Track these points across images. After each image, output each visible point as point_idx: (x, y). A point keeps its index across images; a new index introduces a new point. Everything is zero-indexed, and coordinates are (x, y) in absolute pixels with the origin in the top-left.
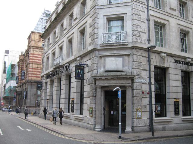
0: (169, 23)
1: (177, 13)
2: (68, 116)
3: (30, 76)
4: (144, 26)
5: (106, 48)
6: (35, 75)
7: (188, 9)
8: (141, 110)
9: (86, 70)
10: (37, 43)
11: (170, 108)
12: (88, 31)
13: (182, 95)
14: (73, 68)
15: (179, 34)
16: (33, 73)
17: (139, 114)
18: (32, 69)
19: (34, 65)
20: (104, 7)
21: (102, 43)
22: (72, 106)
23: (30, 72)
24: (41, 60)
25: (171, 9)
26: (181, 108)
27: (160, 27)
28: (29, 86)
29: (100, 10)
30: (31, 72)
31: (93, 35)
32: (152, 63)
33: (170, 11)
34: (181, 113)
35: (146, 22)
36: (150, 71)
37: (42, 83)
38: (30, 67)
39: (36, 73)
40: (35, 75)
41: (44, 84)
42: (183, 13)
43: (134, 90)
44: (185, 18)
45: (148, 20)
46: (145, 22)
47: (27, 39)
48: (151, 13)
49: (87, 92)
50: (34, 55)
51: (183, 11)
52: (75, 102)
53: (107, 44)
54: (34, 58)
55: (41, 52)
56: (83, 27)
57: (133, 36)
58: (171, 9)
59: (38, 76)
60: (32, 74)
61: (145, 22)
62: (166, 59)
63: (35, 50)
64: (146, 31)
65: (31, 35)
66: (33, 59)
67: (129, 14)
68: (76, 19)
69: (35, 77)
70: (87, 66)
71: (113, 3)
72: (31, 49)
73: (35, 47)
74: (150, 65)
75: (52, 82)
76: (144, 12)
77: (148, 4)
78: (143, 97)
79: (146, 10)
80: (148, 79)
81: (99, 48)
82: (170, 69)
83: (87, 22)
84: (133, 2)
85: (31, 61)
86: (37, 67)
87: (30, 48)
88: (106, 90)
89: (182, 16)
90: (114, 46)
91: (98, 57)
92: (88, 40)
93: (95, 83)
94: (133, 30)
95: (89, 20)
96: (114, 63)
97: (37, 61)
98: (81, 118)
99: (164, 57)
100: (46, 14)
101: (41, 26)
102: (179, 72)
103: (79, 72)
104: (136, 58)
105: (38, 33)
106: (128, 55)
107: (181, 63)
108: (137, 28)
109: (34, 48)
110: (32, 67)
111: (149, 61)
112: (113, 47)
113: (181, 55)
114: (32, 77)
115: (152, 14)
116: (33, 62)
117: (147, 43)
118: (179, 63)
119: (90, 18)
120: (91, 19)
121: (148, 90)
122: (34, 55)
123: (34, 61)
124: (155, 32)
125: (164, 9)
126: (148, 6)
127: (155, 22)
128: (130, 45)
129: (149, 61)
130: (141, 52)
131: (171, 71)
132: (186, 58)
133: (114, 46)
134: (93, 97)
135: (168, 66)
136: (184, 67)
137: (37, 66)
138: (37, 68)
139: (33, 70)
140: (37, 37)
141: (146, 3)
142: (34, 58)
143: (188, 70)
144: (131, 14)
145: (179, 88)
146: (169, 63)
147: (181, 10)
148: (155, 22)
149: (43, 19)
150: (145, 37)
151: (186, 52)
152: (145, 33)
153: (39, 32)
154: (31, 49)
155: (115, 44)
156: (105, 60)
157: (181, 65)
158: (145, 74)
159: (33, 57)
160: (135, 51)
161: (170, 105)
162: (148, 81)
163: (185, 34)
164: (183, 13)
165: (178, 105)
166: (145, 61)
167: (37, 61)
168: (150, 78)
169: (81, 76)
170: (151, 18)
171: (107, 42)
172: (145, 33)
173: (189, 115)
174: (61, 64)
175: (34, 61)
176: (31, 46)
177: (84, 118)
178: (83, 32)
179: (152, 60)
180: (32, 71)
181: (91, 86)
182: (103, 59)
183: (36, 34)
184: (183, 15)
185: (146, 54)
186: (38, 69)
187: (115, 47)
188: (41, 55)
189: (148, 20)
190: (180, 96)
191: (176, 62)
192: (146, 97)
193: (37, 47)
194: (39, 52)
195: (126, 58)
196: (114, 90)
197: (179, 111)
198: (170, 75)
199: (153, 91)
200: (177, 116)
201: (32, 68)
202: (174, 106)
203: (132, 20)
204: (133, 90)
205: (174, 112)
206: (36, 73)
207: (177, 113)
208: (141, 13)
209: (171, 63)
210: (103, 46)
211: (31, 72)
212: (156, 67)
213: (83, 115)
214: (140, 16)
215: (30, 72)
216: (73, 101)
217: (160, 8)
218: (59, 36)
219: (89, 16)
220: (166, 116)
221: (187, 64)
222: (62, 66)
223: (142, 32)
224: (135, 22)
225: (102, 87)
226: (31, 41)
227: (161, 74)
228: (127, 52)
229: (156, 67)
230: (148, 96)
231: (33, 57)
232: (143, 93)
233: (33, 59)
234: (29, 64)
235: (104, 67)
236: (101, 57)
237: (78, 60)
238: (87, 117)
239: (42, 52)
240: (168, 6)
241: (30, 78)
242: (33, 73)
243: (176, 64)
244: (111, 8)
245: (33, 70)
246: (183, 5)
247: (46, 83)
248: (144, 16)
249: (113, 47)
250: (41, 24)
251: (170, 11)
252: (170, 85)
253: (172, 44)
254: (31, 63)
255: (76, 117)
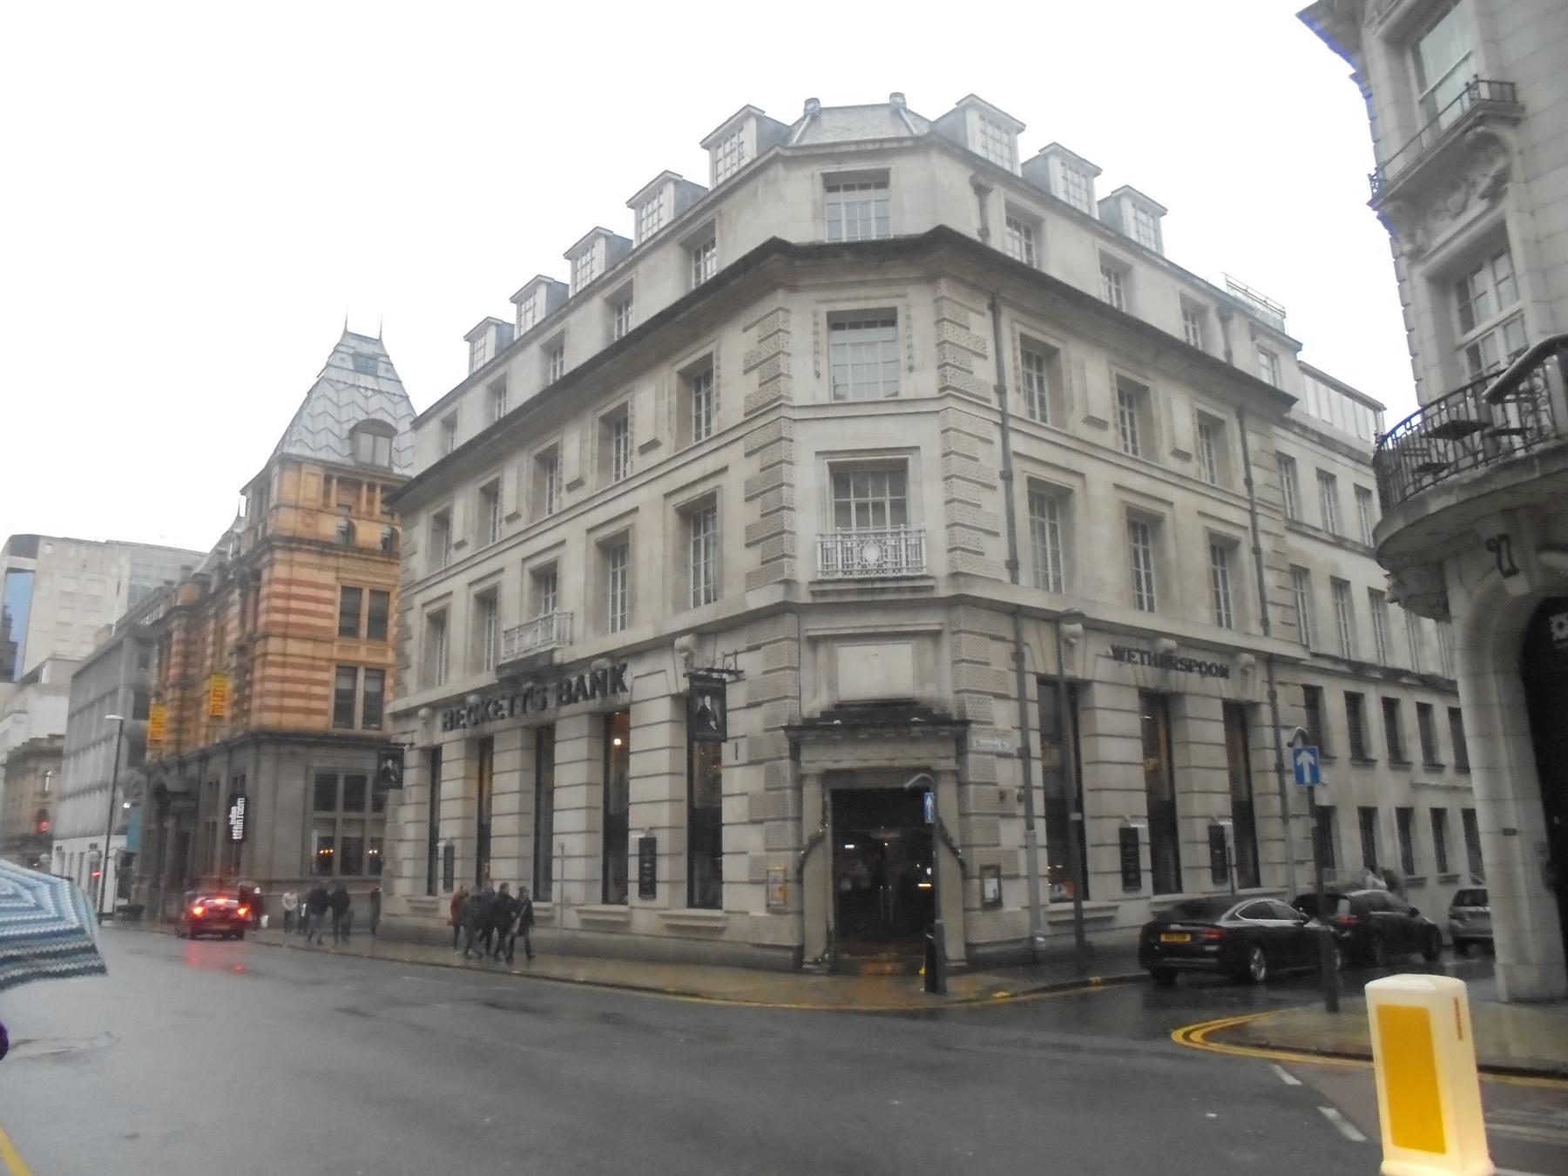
0: (1085, 486)
1: (1109, 438)
2: (720, 924)
3: (269, 709)
4: (993, 504)
5: (835, 599)
6: (301, 703)
7: (1155, 413)
8: (995, 870)
9: (736, 695)
10: (309, 520)
11: (1104, 859)
12: (736, 516)
13: (1148, 802)
14: (654, 691)
15: (1122, 527)
16: (288, 687)
17: (991, 886)
18: (284, 665)
19: (294, 647)
20: (817, 413)
21: (820, 577)
22: (641, 868)
23: (268, 686)
24: (330, 616)
25: (1092, 421)
26: (1145, 860)
27: (1051, 501)
28: (267, 765)
29: (798, 425)
30: (276, 687)
31: (771, 538)
32: (1028, 666)
33: (1174, 464)
34: (1147, 880)
35: (1000, 484)
36: (1022, 699)
37: (402, 751)
38: (270, 658)
39: (301, 688)
40: (301, 703)
41: (412, 758)
42: (1133, 434)
43: (968, 783)
44: (1140, 457)
45: (1007, 476)
46: (993, 488)
47: (243, 492)
48: (1017, 444)
49: (746, 799)
50: (295, 590)
51: (1132, 424)
52: (457, 854)
53: (839, 581)
54: (294, 604)
55: (329, 568)
56: (701, 490)
57: (951, 550)
58: (1092, 421)
59: (315, 704)
60: (283, 694)
61: (993, 488)
62: (1079, 644)
63: (298, 557)
64: (1002, 528)
65: (276, 470)
66: (288, 611)
67: (931, 450)
68: (653, 444)
69: (297, 710)
70: (738, 680)
71: (850, 399)
72: (279, 555)
73: (300, 540)
74: (1020, 672)
75: (482, 750)
76: (990, 442)
77: (1002, 403)
78: (1003, 816)
79: (996, 436)
80: (1017, 733)
81: (804, 597)
82: (1096, 686)
83: (725, 469)
84: (950, 402)
85: (277, 624)
86: (290, 642)
87: (272, 549)
88: (841, 784)
89: (1130, 445)
90: (873, 591)
91: (798, 640)
92: (738, 557)
93: (795, 755)
94: (955, 524)
95: (740, 470)
96: (874, 670)
97: (312, 621)
98: (713, 924)
99: (1075, 636)
100: (356, 356)
101: (330, 422)
102: (1132, 700)
103: (704, 707)
104: (970, 646)
105: (315, 461)
106: (935, 635)
107: (1137, 657)
108: (962, 514)
109: (292, 550)
110: (285, 655)
111: (1018, 657)
112: (868, 598)
113: (1136, 624)
114: (282, 709)
115: (1022, 450)
116: (287, 625)
117: (1006, 577)
118: (1129, 661)
119: (748, 455)
120: (755, 463)
121: (1020, 781)
122: (295, 590)
123: (293, 618)
124: (1032, 522)
125: (1064, 424)
126: (1004, 415)
127: (1032, 482)
128: (944, 591)
129: (1018, 657)
130: (985, 621)
131: (1101, 696)
132: (1157, 635)
133: (873, 591)
134: (785, 819)
135: (1088, 677)
136: (1148, 676)
137: (308, 648)
138: (280, 659)
139: (289, 672)
140: (311, 486)
141: (995, 404)
142: (294, 604)
143: (1165, 688)
144: (938, 452)
145: (1133, 768)
146: (1091, 662)
147: (1123, 421)
148: (1032, 482)
149: (341, 386)
150: (997, 551)
151: (1151, 609)
152: (996, 534)
153: (322, 455)
154: (279, 555)
155: (878, 585)
156: (833, 658)
157: (1139, 667)
158: (1003, 715)
159: (289, 597)
160: (963, 619)
161: (1103, 845)
162: (1018, 744)
163: (1144, 528)
164: (1133, 434)
165: (1136, 844)
166: (999, 656)
167: (312, 621)
168: (1023, 727)
169: (713, 724)
170: (1017, 466)
171: (840, 575)
172: (996, 534)
173: (1174, 887)
174: (558, 658)
175: (293, 618)
176: (280, 538)
177: (726, 919)
178: (697, 515)
179: (1026, 650)
180: (284, 680)
181: (773, 775)
182: (822, 651)
183: (306, 468)
184: (1134, 441)
185: (1004, 627)
186: (313, 668)
187: (877, 598)
188: (332, 588)
189: (1007, 476)
190: (1140, 803)
191: (1119, 655)
192: (1014, 816)
193: (310, 542)
194: (321, 568)
195: (927, 644)
196: (907, 785)
197: (1137, 871)
198: (1099, 713)
199: (1297, 816)
200: (1132, 895)
201: (280, 659)
202: (1117, 851)
203: (946, 479)
204: (961, 784)
205: (1118, 879)
206: (301, 688)
207: (1130, 878)
208: (980, 450)
209: (1101, 661)
210: (825, 593)
211: (276, 687)
212: (1043, 681)
213: (720, 908)
214: (976, 459)
215: (268, 686)
216: (648, 846)
217: (1044, 419)
218: (525, 513)
219: (740, 448)
220: (1179, 889)
221: (1166, 661)
222: (563, 669)
223: (988, 532)
224: (962, 490)
225: (827, 776)
226: (277, 507)
227: (1065, 701)
228: (930, 621)
229: (1043, 681)
230: (1020, 810)
231: (289, 597)
232: (1002, 796)
233: (288, 611)
234: (266, 636)
235: (832, 685)
236: (814, 642)
237: (683, 650)
238: (753, 913)
239: (337, 569)
240: (1077, 408)
241: (270, 719)
242: (288, 687)
243: (1115, 663)
244: (847, 421)
245: (289, 672)
246: (1129, 396)
247: (433, 756)
248: (990, 461)
249: (868, 598)
250: (331, 408)
251: (1174, 464)
252: (1102, 758)
253: (1101, 577)
254: (280, 631)
255: (669, 922)
